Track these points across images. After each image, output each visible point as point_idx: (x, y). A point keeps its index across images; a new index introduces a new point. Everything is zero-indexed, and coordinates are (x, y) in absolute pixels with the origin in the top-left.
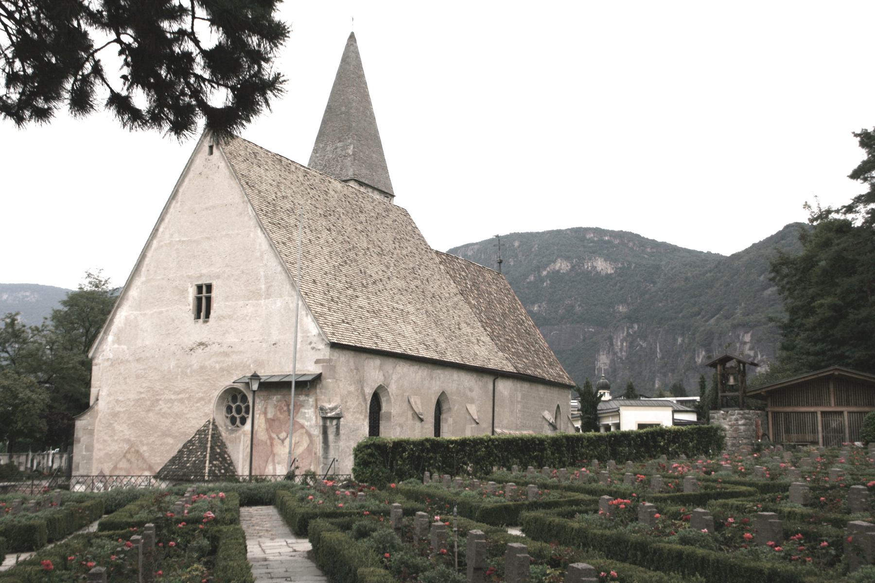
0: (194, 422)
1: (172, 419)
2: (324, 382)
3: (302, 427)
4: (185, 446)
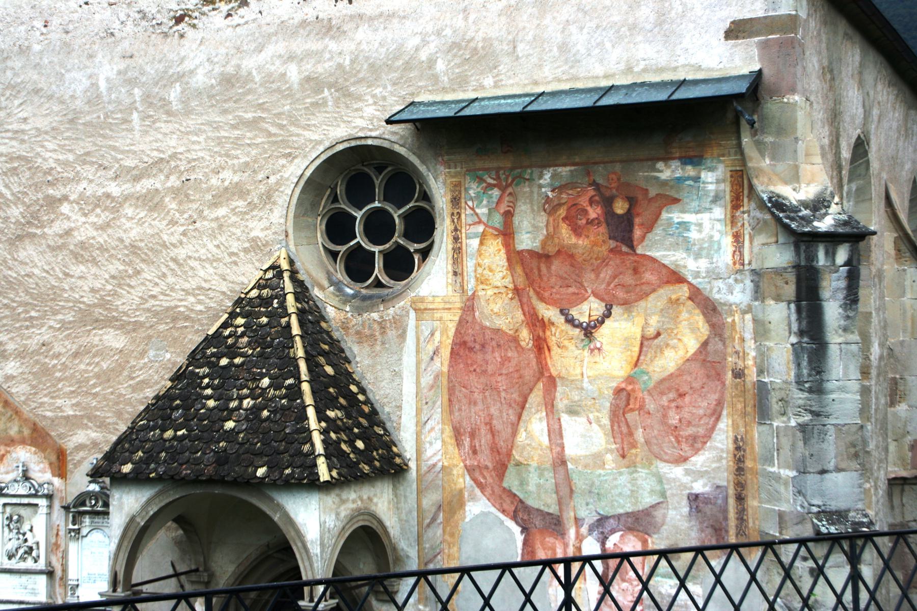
0: (205, 272)
1: (115, 267)
2: (771, 107)
3: (675, 277)
4: (195, 358)
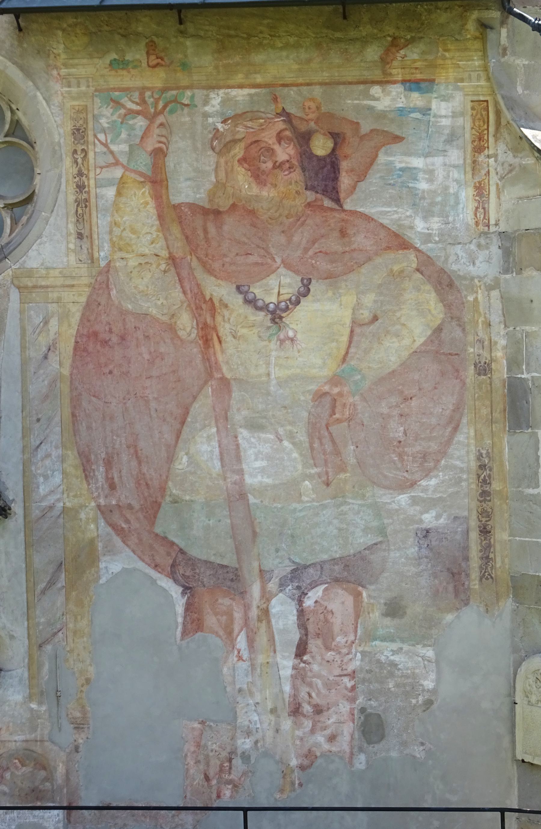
3: (399, 242)
